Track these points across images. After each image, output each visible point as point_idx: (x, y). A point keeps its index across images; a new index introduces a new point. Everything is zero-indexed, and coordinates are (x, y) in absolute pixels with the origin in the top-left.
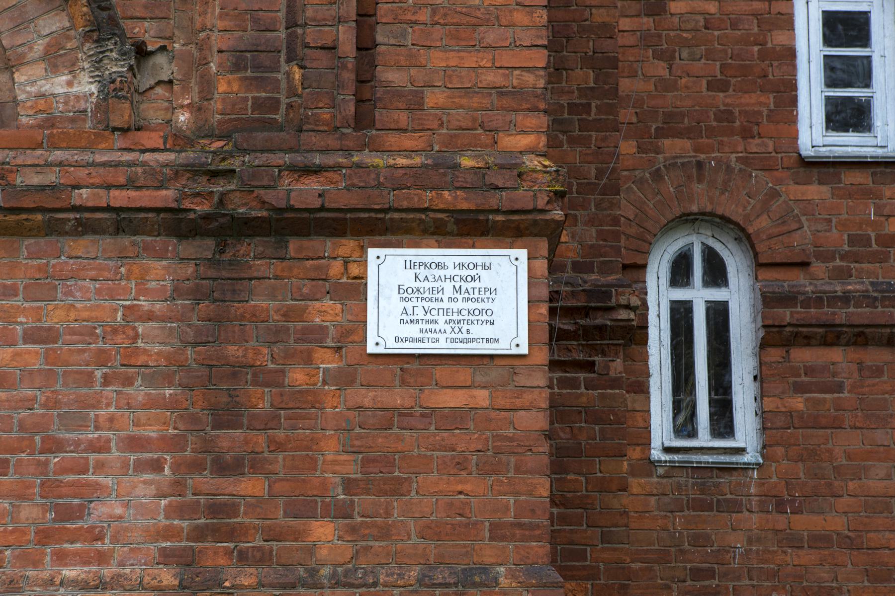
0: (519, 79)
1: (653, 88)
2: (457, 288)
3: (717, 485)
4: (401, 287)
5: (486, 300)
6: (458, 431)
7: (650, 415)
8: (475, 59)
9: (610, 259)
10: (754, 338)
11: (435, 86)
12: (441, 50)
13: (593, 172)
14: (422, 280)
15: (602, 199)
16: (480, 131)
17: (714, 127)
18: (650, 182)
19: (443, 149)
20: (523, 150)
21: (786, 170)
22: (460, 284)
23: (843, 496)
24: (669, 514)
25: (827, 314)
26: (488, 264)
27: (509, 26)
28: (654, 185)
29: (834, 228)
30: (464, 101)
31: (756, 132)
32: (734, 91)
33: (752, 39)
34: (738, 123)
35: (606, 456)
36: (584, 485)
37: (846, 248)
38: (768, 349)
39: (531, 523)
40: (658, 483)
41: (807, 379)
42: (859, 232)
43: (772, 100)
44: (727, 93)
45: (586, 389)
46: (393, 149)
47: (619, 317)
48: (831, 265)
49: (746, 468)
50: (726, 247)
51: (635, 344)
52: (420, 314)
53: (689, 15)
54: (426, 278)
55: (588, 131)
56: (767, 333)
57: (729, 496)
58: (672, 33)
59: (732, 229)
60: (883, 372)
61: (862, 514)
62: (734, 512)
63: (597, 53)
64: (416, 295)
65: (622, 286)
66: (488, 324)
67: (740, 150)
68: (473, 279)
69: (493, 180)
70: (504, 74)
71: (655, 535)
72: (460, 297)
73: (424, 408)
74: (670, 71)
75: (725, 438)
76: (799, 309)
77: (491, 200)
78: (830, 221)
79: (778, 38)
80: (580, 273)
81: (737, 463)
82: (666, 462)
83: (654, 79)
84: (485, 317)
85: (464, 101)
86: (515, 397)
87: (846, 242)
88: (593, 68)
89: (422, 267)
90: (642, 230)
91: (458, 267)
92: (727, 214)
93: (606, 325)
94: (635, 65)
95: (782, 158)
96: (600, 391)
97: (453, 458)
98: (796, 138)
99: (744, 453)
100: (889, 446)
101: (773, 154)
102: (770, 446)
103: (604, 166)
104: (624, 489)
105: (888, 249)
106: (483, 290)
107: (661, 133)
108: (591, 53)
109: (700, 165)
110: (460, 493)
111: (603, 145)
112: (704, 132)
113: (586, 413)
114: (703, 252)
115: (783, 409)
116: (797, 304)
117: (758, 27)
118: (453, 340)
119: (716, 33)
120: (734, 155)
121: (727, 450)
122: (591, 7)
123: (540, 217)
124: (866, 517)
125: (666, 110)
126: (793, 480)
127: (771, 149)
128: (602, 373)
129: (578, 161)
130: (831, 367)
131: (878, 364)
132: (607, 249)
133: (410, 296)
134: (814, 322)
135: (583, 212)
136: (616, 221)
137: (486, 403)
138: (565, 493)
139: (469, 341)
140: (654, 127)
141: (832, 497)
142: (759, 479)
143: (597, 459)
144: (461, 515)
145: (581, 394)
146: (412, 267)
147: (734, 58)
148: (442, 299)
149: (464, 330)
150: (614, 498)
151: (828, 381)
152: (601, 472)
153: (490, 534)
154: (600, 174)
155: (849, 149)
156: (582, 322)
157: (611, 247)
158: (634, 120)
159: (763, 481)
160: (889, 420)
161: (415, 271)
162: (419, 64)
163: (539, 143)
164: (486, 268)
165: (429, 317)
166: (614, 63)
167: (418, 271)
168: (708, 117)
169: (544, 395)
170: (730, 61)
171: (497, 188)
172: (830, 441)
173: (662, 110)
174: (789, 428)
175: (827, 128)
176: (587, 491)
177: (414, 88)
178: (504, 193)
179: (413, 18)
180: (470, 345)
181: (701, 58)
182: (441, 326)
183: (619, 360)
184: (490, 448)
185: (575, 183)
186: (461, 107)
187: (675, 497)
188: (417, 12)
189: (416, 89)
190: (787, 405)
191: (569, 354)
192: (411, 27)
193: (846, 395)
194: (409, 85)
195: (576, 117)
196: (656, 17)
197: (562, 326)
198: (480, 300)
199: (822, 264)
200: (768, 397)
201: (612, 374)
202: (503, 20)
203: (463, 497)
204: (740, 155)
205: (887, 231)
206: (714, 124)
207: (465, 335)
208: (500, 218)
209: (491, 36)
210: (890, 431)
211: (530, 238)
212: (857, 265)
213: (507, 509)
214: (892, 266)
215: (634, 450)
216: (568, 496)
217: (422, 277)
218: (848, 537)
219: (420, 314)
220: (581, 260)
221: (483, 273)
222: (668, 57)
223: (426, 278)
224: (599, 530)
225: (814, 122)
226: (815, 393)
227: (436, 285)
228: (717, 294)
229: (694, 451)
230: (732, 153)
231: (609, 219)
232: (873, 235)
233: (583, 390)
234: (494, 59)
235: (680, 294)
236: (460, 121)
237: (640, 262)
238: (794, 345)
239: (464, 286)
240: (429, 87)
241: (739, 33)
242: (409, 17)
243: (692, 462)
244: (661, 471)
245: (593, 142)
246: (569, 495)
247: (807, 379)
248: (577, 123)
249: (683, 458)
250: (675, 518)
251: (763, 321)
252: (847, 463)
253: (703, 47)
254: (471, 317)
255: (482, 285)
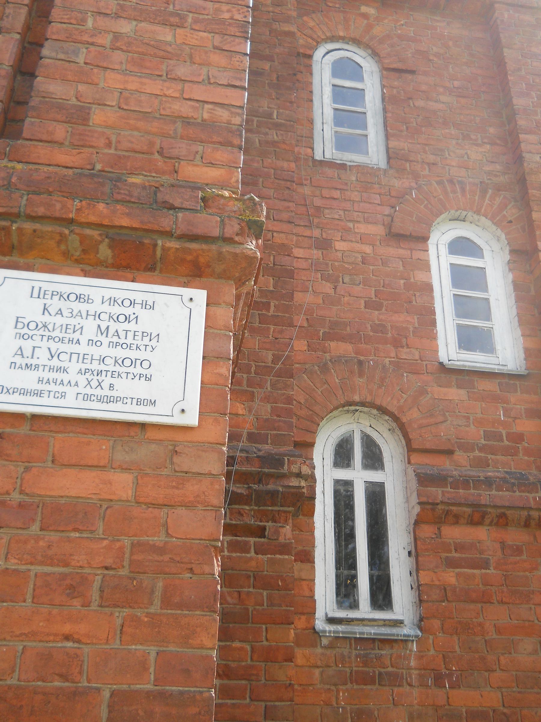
0: (211, 113)
1: (321, 301)
2: (103, 328)
3: (379, 658)
4: (20, 320)
5: (142, 348)
6: (77, 535)
7: (314, 584)
8: (160, 87)
9: (283, 433)
10: (408, 517)
11: (105, 105)
12: (119, 73)
13: (270, 358)
14: (53, 312)
15: (277, 380)
16: (157, 156)
17: (371, 336)
18: (318, 373)
19: (107, 169)
20: (210, 182)
21: (430, 374)
22: (109, 324)
23: (496, 670)
24: (333, 688)
25: (474, 495)
26: (150, 303)
27: (204, 65)
28: (322, 376)
29: (472, 425)
30: (140, 124)
31: (404, 343)
32: (386, 310)
33: (399, 274)
34: (390, 335)
35: (274, 623)
36: (249, 653)
37: (483, 442)
38: (421, 525)
39: (181, 693)
40: (323, 654)
41: (457, 555)
42: (492, 429)
43: (416, 320)
44: (381, 312)
45: (256, 553)
46: (40, 162)
47: (291, 484)
48: (471, 455)
49: (405, 641)
50: (382, 435)
51: (304, 515)
52: (42, 357)
53: (350, 252)
54: (60, 312)
55: (268, 324)
56: (422, 510)
57: (390, 669)
58: (336, 264)
59: (385, 420)
60: (522, 551)
61: (514, 689)
62: (395, 686)
63: (277, 265)
64: (41, 332)
65: (293, 456)
66: (143, 379)
67: (392, 356)
68: (127, 319)
69: (167, 198)
70: (193, 107)
71: (319, 711)
72: (105, 341)
73: (27, 495)
74: (335, 291)
75: (383, 610)
76: (449, 489)
77: (163, 219)
78: (468, 418)
79: (420, 276)
80: (254, 443)
81: (398, 635)
82: (330, 632)
83: (321, 295)
84: (138, 370)
85: (140, 124)
86: (174, 487)
87: (483, 437)
88: (273, 276)
89: (56, 298)
90: (311, 412)
91: (108, 302)
92: (384, 404)
93: (278, 491)
94: (307, 283)
95: (426, 365)
96: (269, 556)
97: (64, 576)
98: (437, 351)
99: (402, 625)
100: (533, 621)
101: (419, 361)
102: (427, 618)
103: (280, 353)
104: (290, 659)
105: (517, 445)
106: (140, 334)
107: (328, 337)
108: (272, 265)
109: (360, 363)
110: (67, 638)
111: (279, 336)
112: (363, 339)
113: (255, 577)
114: (362, 439)
115: (437, 583)
116: (447, 485)
117: (403, 267)
118: (87, 397)
119: (371, 267)
120: (388, 359)
121: (387, 622)
122: (273, 231)
123: (227, 249)
124: (519, 692)
125: (332, 319)
126: (450, 654)
127: (417, 357)
128: (272, 538)
129: (257, 347)
130: (478, 544)
131: (518, 543)
132: (281, 423)
133: (31, 333)
134: (463, 501)
135: (260, 390)
136: (289, 400)
137: (128, 493)
138: (230, 663)
139: (110, 400)
140: (322, 331)
141: (486, 671)
142: (418, 651)
143: (264, 626)
144: (64, 677)
145: (251, 559)
146: (41, 296)
147: (385, 286)
148: (78, 342)
149: (105, 385)
150: (280, 668)
151: (476, 558)
152: (267, 640)
153: (110, 712)
154: (276, 359)
155: (478, 365)
156: (255, 487)
157: (285, 422)
158: (306, 324)
159: (422, 654)
160: (532, 596)
161: (45, 301)
162: (90, 81)
163: (231, 178)
164: (148, 307)
165: (55, 362)
166: (291, 274)
167: (48, 302)
168: (366, 328)
169: (217, 487)
170: (382, 289)
171: (172, 207)
172: (481, 615)
173: (328, 319)
174: (444, 601)
175: (460, 347)
176: (252, 659)
177: (79, 103)
178: (180, 215)
179: (90, 40)
180: (111, 406)
181: (360, 284)
182: (72, 376)
183: (288, 527)
184: (126, 563)
185: (254, 366)
186: (137, 129)
187: (338, 669)
188: (96, 36)
189: (82, 104)
190: (441, 578)
191: (241, 518)
192: (87, 48)
193: (492, 571)
194: (74, 99)
195: (257, 312)
196: (324, 252)
197: (235, 490)
198: (134, 347)
199: (464, 454)
200: (423, 570)
201: (282, 540)
202: (198, 58)
203: (70, 644)
204: (393, 359)
205: (514, 430)
206: (371, 334)
207: (106, 392)
208: (173, 244)
209: (182, 71)
210: (533, 606)
211: (211, 280)
212: (493, 457)
213: (144, 666)
214: (521, 459)
215: (300, 619)
216: (232, 665)
217: (53, 310)
218: (504, 714)
219: (42, 357)
220: (256, 432)
221: (143, 314)
222: (334, 281)
223: (60, 312)
224: (263, 704)
225: (449, 341)
226: (465, 568)
227: (73, 322)
228: (375, 476)
229: (355, 622)
230: (386, 357)
231: (283, 397)
232: (504, 433)
233: (252, 554)
234: (183, 91)
235: (343, 474)
236: (132, 142)
237: (309, 440)
238: (445, 522)
239: (114, 327)
240: (99, 105)
241: (389, 269)
242: (86, 38)
243: (355, 633)
244: (325, 642)
245: (271, 333)
246: (233, 665)
247: (457, 555)
248: (257, 316)
249: (347, 629)
250: (338, 691)
251: (418, 499)
252: (497, 637)
253: (361, 276)
254: (117, 368)
255: (140, 328)
